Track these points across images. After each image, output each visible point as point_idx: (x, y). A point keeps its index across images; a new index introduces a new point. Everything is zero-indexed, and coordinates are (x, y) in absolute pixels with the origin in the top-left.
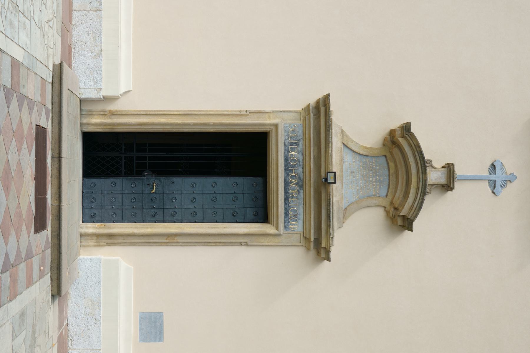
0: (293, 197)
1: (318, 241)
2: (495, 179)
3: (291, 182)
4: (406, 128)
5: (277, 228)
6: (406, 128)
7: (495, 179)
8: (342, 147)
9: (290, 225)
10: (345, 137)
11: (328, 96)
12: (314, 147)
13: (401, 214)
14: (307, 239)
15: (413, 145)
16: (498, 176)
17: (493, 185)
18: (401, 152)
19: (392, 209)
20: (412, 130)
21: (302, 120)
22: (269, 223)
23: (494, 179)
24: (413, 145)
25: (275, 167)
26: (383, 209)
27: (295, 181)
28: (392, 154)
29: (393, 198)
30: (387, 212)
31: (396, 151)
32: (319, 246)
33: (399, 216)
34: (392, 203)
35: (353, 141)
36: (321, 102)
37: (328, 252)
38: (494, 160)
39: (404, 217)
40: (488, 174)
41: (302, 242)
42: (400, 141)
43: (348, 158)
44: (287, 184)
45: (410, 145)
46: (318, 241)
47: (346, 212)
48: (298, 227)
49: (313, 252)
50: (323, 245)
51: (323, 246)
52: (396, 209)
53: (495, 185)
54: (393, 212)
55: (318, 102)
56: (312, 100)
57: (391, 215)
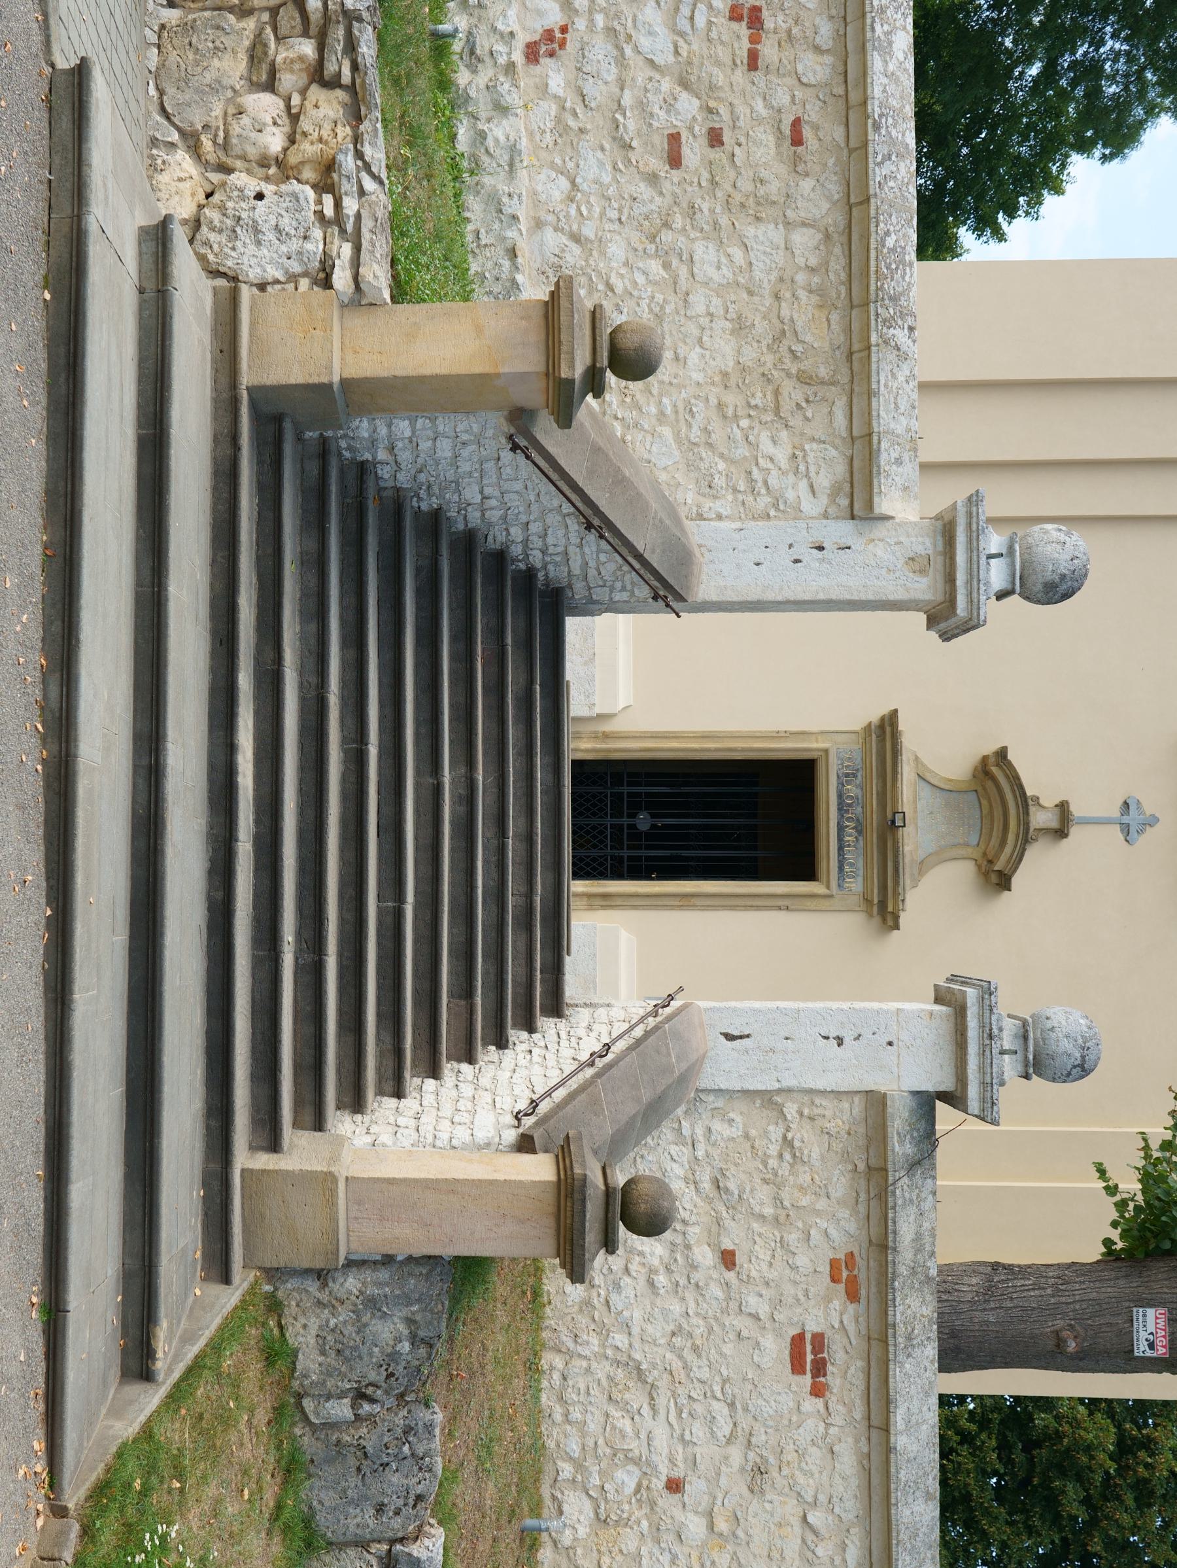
0: (849, 846)
1: (883, 904)
2: (1131, 821)
4: (1002, 754)
5: (828, 887)
6: (1002, 754)
13: (996, 868)
14: (868, 901)
16: (1133, 818)
17: (1126, 830)
18: (994, 779)
30: (979, 867)
34: (985, 854)
37: (896, 918)
39: (999, 872)
43: (925, 792)
44: (841, 829)
45: (1007, 776)
46: (883, 904)
47: (923, 867)
48: (855, 885)
49: (877, 920)
50: (890, 909)
55: (883, 719)
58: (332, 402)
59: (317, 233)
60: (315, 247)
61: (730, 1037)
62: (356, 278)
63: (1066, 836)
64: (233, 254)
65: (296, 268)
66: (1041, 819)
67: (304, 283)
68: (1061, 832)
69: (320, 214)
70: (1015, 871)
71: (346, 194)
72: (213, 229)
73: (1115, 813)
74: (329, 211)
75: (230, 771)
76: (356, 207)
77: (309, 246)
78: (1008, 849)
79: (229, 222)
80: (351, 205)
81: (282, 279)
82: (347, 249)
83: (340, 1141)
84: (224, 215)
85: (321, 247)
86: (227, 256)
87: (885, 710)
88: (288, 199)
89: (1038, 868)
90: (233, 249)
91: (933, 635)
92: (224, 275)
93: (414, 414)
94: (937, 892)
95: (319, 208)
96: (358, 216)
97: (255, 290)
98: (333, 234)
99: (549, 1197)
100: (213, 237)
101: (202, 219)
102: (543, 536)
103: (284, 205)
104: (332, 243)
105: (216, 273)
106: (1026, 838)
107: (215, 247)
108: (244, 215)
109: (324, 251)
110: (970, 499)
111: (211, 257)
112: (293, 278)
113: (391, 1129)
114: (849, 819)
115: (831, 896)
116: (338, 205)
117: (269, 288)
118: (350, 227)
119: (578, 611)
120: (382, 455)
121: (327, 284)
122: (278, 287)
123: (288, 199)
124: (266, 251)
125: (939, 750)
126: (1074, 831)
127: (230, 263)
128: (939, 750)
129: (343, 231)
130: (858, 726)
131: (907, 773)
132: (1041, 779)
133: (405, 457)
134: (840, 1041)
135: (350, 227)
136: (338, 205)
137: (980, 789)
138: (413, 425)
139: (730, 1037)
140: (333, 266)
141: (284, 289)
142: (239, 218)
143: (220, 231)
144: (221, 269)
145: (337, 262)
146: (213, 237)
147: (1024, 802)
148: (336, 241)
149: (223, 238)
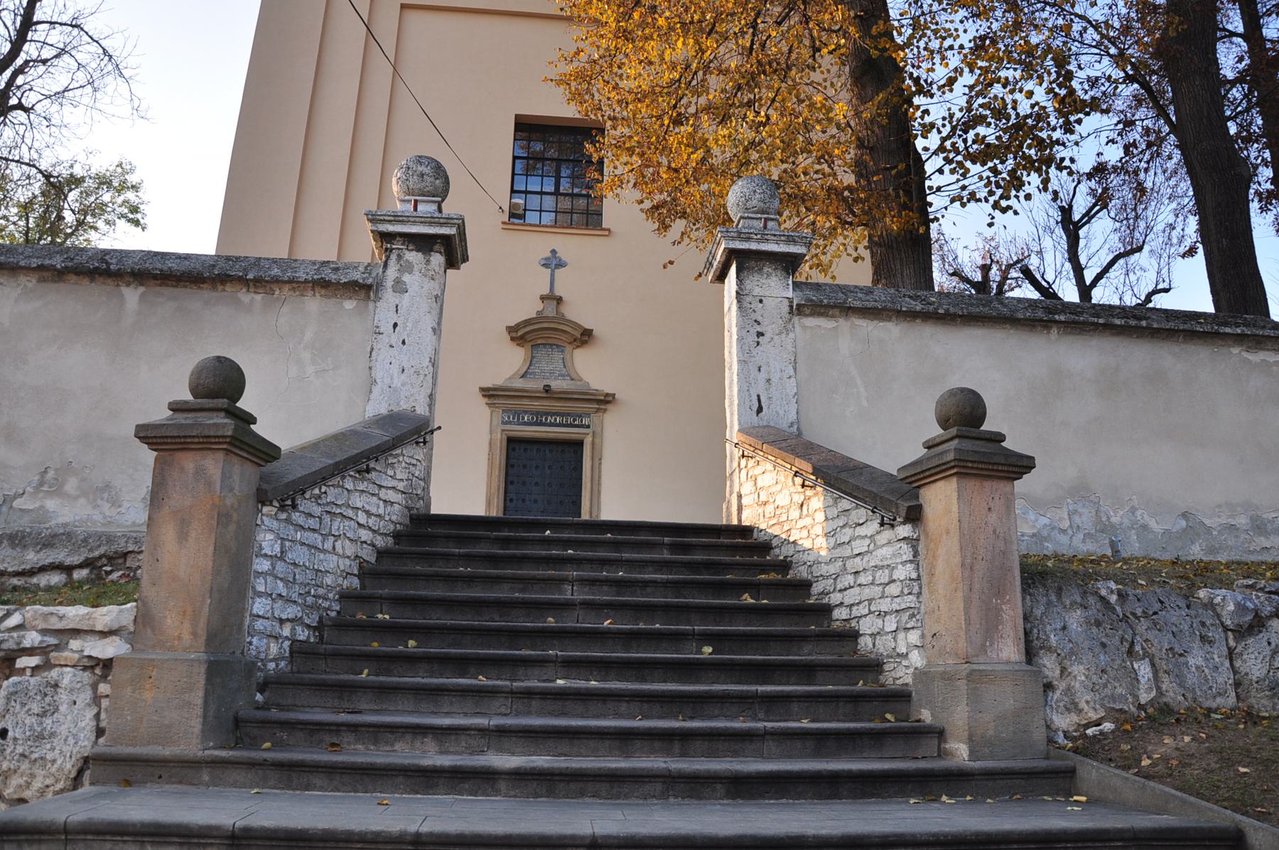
1: (599, 402)
14: (598, 410)
18: (521, 334)
37: (607, 395)
46: (599, 402)
49: (608, 406)
58: (225, 666)
59: (54, 673)
60: (67, 677)
61: (760, 410)
62: (104, 634)
64: (59, 762)
65: (87, 695)
66: (550, 311)
67: (104, 688)
68: (559, 300)
69: (35, 670)
70: (580, 326)
71: (18, 644)
72: (28, 784)
74: (33, 661)
76: (34, 634)
77: (65, 682)
78: (568, 329)
79: (25, 766)
80: (32, 639)
81: (95, 711)
82: (75, 644)
83: (920, 674)
84: (15, 771)
85: (68, 669)
86: (60, 769)
87: (479, 395)
88: (13, 703)
89: (579, 312)
90: (54, 761)
91: (463, 266)
92: (80, 772)
93: (251, 594)
94: (591, 369)
95: (28, 672)
96: (44, 632)
97: (101, 740)
98: (56, 658)
99: (971, 484)
100: (37, 784)
101: (16, 796)
102: (368, 513)
103: (18, 707)
104: (66, 659)
105: (77, 782)
106: (561, 318)
107: (48, 782)
108: (20, 750)
109: (73, 666)
110: (370, 220)
111: (60, 786)
112: (96, 699)
113: (901, 635)
116: (30, 652)
117: (103, 724)
118: (52, 640)
119: (428, 506)
120: (286, 631)
121: (107, 664)
122: (103, 716)
123: (13, 703)
124: (63, 727)
125: (507, 364)
126: (558, 293)
127: (69, 766)
128: (507, 364)
129: (57, 647)
130: (487, 411)
131: (519, 384)
132: (527, 308)
133: (291, 611)
134: (760, 334)
135: (52, 640)
136: (30, 652)
138: (260, 595)
139: (760, 410)
140: (90, 657)
141: (106, 710)
142: (23, 755)
143: (33, 776)
144: (73, 775)
145: (86, 653)
146: (37, 784)
147: (540, 317)
148: (66, 654)
149: (40, 772)
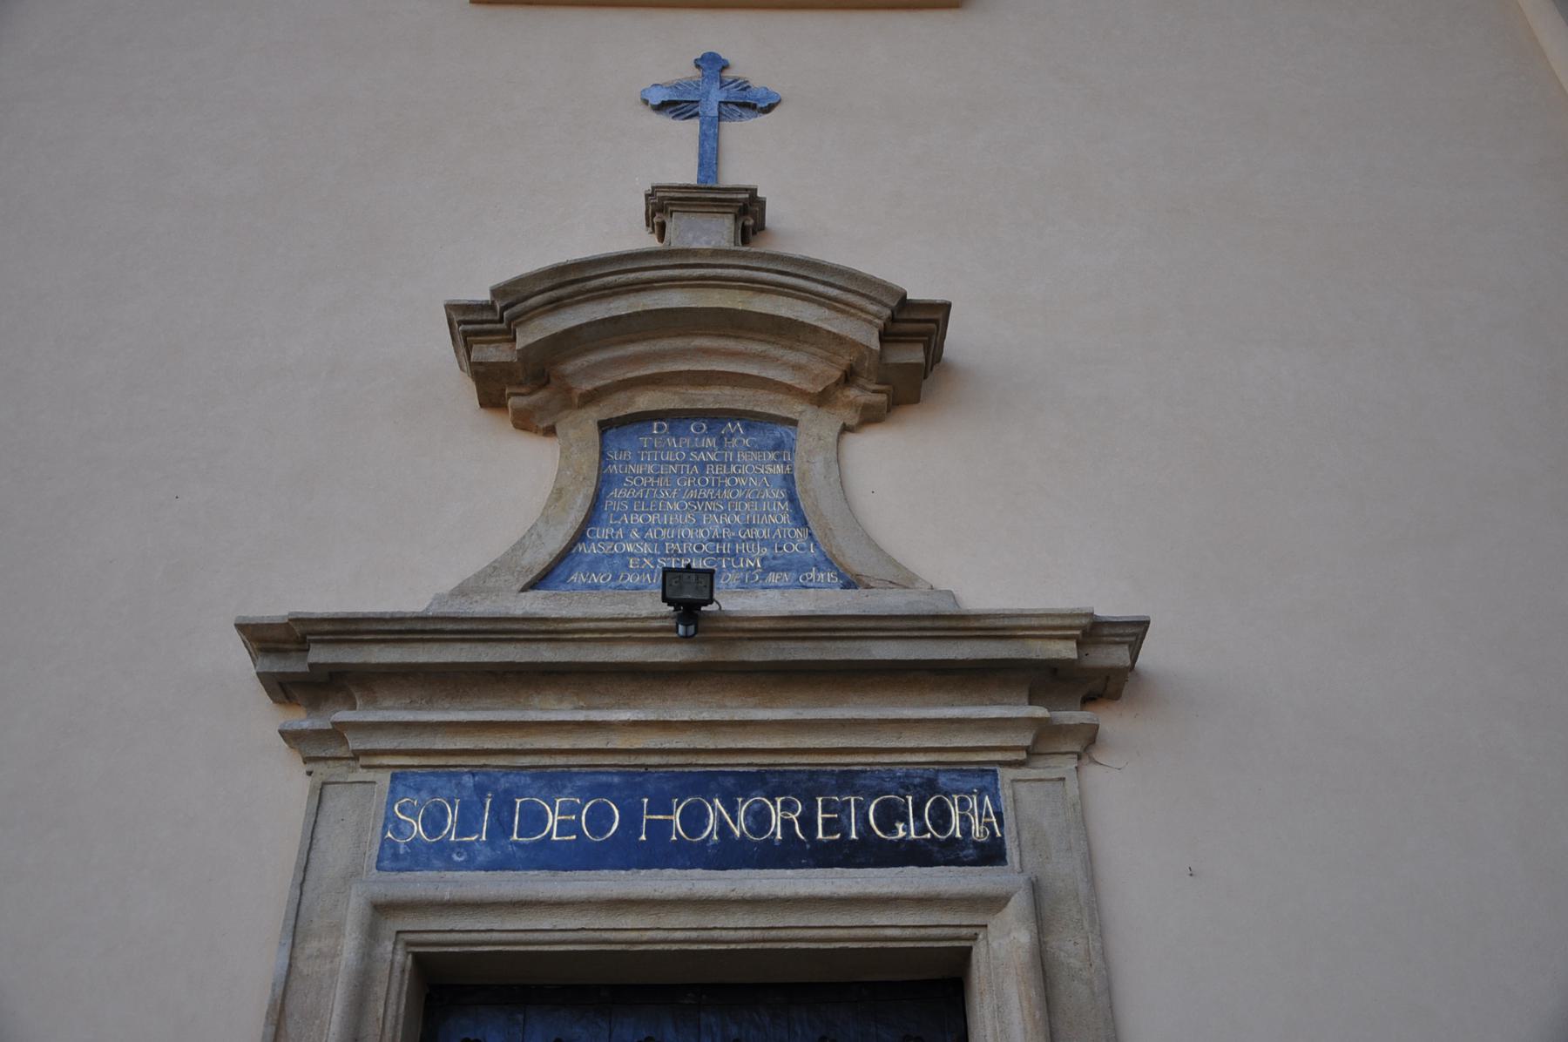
0: (808, 822)
1: (1046, 680)
2: (714, 99)
3: (723, 828)
5: (995, 903)
6: (471, 325)
7: (714, 99)
8: (542, 593)
9: (967, 831)
10: (491, 583)
11: (242, 628)
12: (527, 707)
13: (875, 344)
15: (553, 294)
19: (852, 393)
20: (481, 294)
21: (369, 775)
22: (965, 955)
23: (716, 105)
24: (553, 294)
25: (629, 921)
26: (850, 438)
27: (715, 809)
28: (591, 398)
29: (801, 394)
30: (871, 417)
31: (582, 371)
32: (1080, 675)
33: (881, 356)
34: (822, 399)
35: (519, 546)
36: (301, 719)
37: (1093, 631)
38: (641, 107)
39: (885, 337)
40: (696, 122)
41: (1055, 774)
42: (531, 340)
45: (556, 305)
46: (1046, 680)
49: (1110, 721)
50: (1066, 650)
51: (1074, 655)
52: (849, 377)
53: (737, 104)
54: (863, 389)
55: (282, 689)
56: (267, 719)
57: (882, 398)
63: (753, 191)
73: (690, 129)
75: (951, 721)
87: (236, 639)
114: (694, 819)
115: (1035, 888)
137: (594, 414)
